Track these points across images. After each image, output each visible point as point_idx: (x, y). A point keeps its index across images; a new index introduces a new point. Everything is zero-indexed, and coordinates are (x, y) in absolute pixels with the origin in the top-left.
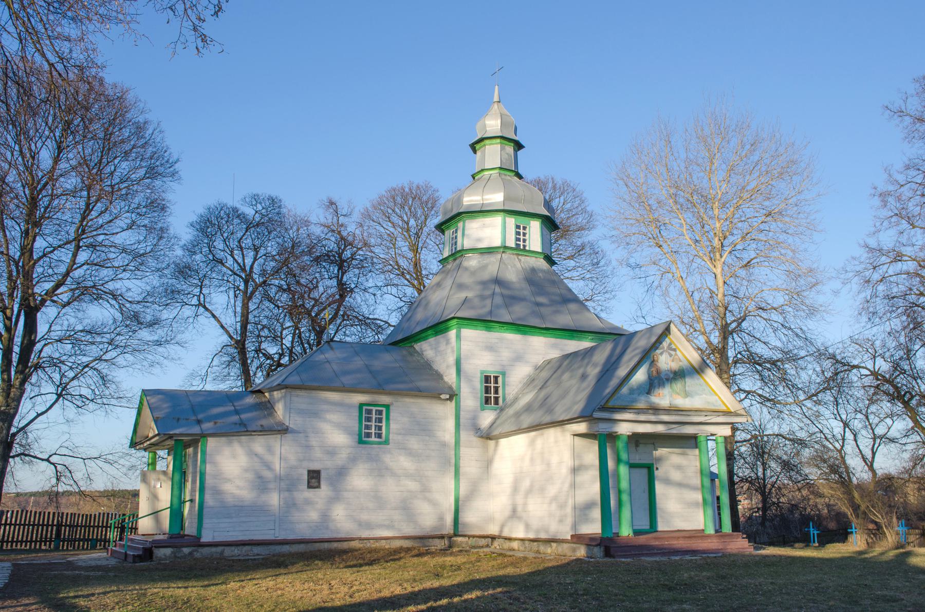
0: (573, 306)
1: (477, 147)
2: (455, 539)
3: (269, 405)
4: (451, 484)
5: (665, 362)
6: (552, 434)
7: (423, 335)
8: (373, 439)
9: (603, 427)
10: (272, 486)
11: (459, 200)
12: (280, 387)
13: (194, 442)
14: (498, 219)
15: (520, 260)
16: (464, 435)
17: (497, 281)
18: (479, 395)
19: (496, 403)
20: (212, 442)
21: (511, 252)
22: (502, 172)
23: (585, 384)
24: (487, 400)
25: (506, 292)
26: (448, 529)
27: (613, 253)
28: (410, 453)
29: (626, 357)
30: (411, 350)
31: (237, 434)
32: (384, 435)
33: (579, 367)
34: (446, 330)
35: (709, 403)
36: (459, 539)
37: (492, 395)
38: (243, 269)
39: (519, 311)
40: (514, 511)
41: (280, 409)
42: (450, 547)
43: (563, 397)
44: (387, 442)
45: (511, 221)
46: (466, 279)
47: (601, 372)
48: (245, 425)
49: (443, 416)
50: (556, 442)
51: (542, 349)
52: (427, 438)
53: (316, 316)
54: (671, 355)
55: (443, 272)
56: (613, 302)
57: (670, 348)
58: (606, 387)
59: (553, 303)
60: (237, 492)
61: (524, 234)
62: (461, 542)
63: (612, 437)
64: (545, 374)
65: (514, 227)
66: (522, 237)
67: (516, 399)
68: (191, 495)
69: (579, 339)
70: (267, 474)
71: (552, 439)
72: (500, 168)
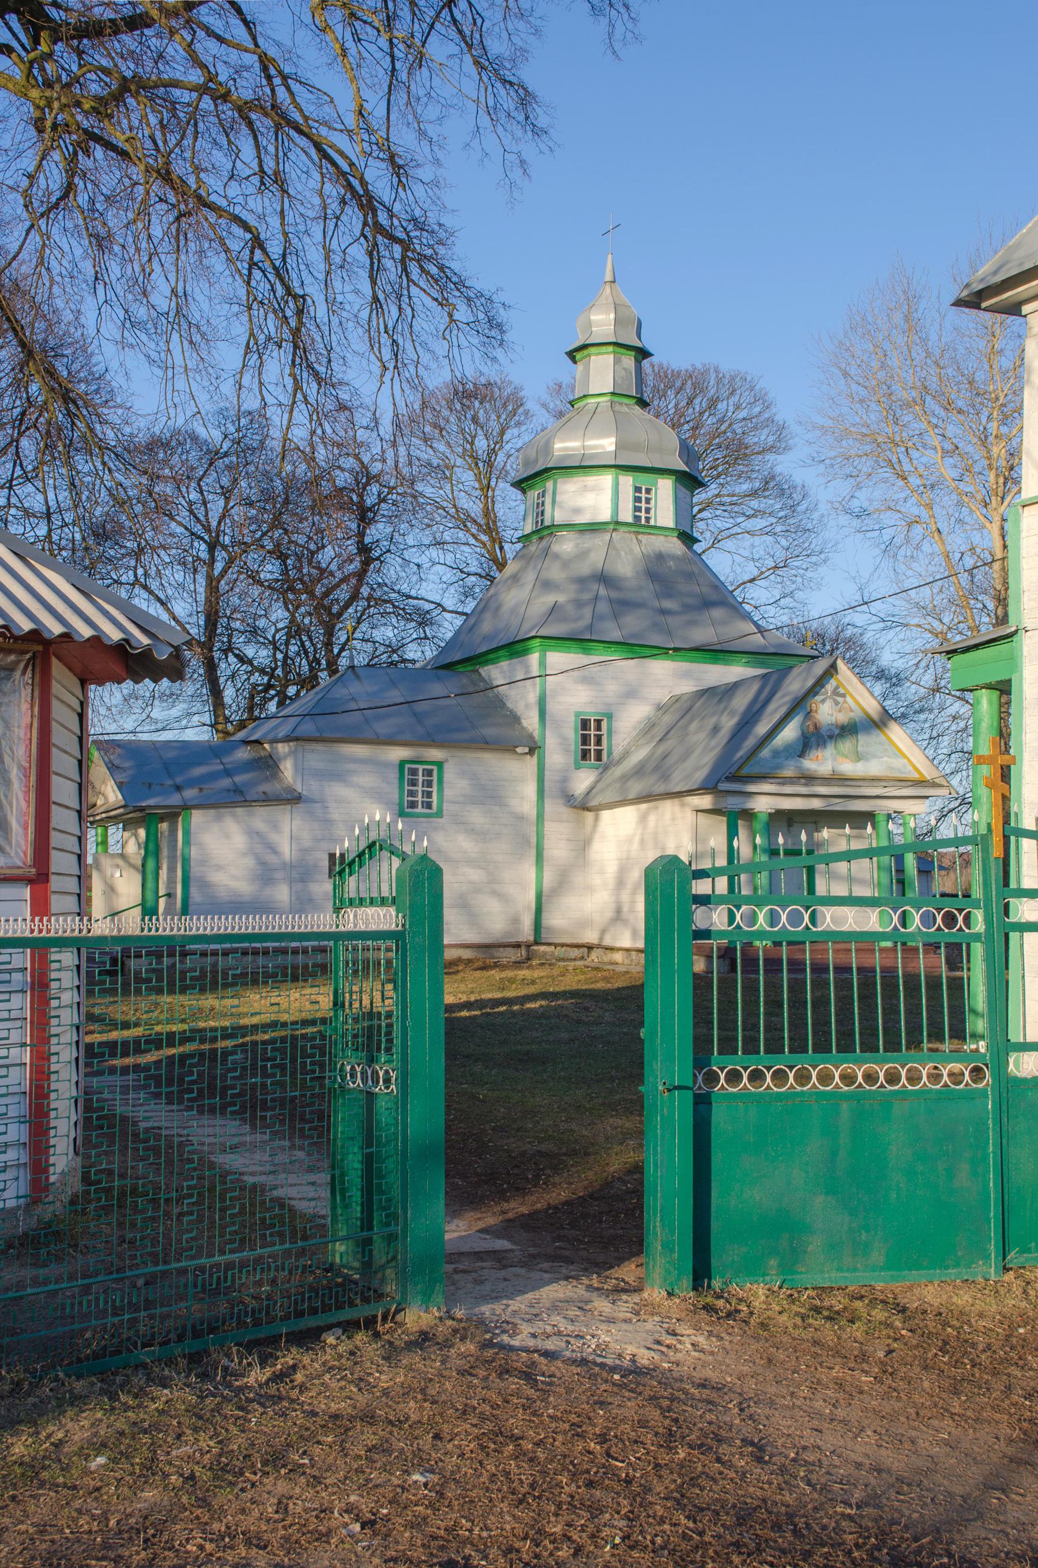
0: (717, 613)
1: (578, 356)
2: (535, 948)
3: (271, 762)
4: (531, 874)
5: (826, 712)
6: (668, 808)
7: (491, 656)
8: (420, 810)
9: (733, 803)
10: (279, 875)
11: (547, 448)
12: (287, 739)
13: (172, 815)
14: (606, 479)
15: (639, 542)
16: (549, 806)
17: (603, 578)
18: (573, 748)
19: (599, 758)
20: (197, 817)
21: (626, 529)
22: (616, 399)
23: (714, 742)
24: (585, 755)
25: (614, 595)
26: (526, 933)
27: (822, 490)
28: (472, 831)
29: (771, 707)
30: (474, 676)
31: (232, 804)
32: (435, 805)
33: (713, 714)
34: (525, 652)
35: (892, 768)
36: (543, 948)
37: (592, 747)
38: (207, 529)
39: (634, 623)
40: (619, 911)
41: (288, 769)
42: (528, 959)
43: (684, 757)
44: (439, 814)
45: (627, 481)
46: (555, 573)
47: (738, 724)
48: (241, 793)
49: (520, 780)
50: (673, 819)
51: (667, 679)
52: (497, 808)
53: (326, 594)
54: (837, 703)
55: (523, 557)
56: (822, 570)
57: (836, 692)
58: (737, 750)
59: (687, 608)
60: (234, 884)
61: (648, 501)
62: (545, 953)
63: (748, 815)
64: (667, 719)
65: (631, 489)
66: (643, 505)
67: (626, 755)
68: (168, 887)
69: (727, 663)
70: (272, 859)
71: (668, 816)
72: (613, 394)
